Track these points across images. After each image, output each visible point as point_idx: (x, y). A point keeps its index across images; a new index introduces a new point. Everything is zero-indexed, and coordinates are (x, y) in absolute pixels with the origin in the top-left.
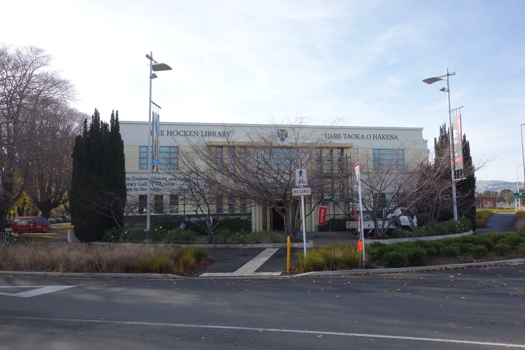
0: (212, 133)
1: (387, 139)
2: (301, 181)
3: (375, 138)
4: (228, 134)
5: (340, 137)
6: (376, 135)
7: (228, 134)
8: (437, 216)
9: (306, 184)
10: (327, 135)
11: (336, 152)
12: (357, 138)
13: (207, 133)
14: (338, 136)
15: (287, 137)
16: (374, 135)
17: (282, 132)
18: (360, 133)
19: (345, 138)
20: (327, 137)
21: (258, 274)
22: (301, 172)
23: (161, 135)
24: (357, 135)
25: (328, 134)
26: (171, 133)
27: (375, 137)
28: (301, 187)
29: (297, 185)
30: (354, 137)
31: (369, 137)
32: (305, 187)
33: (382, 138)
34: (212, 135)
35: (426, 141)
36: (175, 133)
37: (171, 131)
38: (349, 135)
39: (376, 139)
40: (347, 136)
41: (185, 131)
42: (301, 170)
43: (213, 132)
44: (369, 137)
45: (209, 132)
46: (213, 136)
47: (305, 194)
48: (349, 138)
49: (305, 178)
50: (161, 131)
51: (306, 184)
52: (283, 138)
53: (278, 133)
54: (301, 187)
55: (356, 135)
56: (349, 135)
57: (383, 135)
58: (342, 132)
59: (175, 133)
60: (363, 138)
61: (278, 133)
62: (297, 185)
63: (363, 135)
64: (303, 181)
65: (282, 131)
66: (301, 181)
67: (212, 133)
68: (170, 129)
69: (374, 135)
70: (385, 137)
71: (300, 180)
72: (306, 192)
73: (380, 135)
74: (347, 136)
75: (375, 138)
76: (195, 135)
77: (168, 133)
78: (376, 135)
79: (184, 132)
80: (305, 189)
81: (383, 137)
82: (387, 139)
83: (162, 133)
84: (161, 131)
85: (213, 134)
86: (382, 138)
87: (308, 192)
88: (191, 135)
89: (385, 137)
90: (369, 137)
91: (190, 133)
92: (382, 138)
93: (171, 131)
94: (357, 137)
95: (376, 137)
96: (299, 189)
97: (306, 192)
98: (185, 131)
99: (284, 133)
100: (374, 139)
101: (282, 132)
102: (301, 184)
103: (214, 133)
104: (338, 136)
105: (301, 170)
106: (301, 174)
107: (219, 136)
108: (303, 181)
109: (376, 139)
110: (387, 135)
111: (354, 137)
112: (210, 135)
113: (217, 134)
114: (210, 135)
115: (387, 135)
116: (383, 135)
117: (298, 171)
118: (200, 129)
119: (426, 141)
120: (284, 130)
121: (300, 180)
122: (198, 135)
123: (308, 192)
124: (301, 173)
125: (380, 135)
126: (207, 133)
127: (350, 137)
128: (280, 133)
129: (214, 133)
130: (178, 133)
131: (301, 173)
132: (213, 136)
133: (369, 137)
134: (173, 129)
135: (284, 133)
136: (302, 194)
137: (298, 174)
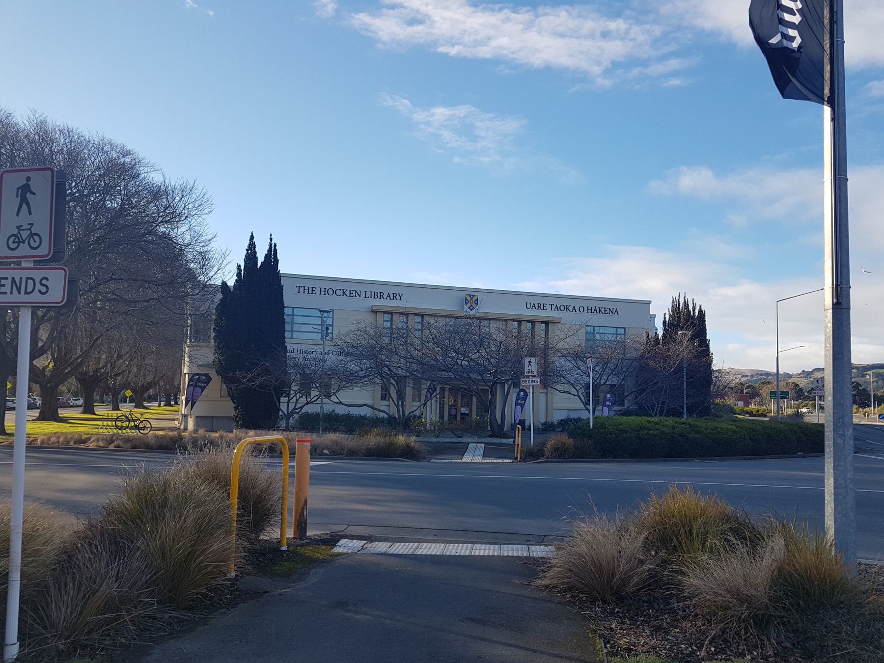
0: (379, 295)
1: (605, 313)
2: (530, 371)
3: (590, 311)
4: (400, 297)
5: (545, 308)
6: (591, 307)
7: (400, 297)
8: (655, 433)
9: (535, 374)
10: (528, 304)
11: (540, 328)
12: (567, 311)
13: (373, 293)
14: (542, 307)
15: (477, 304)
16: (588, 307)
17: (472, 298)
18: (571, 304)
19: (551, 310)
20: (528, 307)
21: (624, 419)
22: (530, 362)
23: (312, 293)
24: (567, 306)
25: (530, 303)
26: (325, 291)
27: (589, 310)
28: (24, 265)
29: (526, 374)
30: (562, 308)
31: (581, 309)
32: (533, 377)
33: (598, 312)
34: (379, 297)
35: (654, 316)
36: (331, 292)
37: (325, 289)
38: (557, 305)
39: (591, 312)
40: (554, 307)
41: (343, 290)
42: (28, 179)
43: (380, 293)
44: (581, 309)
45: (374, 292)
46: (380, 298)
47: (534, 384)
48: (556, 309)
49: (534, 367)
50: (312, 288)
51: (535, 374)
52: (471, 306)
53: (466, 299)
54: (19, 263)
55: (566, 307)
56: (557, 305)
57: (599, 308)
58: (548, 302)
59: (331, 292)
60: (574, 311)
61: (466, 299)
62: (526, 374)
63: (574, 307)
64: (32, 235)
65: (472, 297)
66: (530, 371)
67: (379, 295)
68: (324, 285)
69: (588, 307)
70: (603, 310)
71: (18, 227)
72: (13, 280)
73: (595, 308)
74: (554, 307)
75: (590, 311)
76: (357, 295)
77: (321, 291)
78: (591, 307)
79: (342, 291)
80: (534, 379)
81: (600, 310)
82: (605, 313)
83: (312, 290)
84: (312, 288)
85: (380, 296)
86: (598, 312)
87: (44, 289)
88: (351, 295)
89: (603, 310)
90: (581, 309)
91: (350, 293)
92: (598, 312)
93: (325, 289)
94: (567, 308)
95: (591, 310)
96: (528, 379)
97: (13, 280)
98: (343, 290)
99: (474, 299)
100: (588, 312)
101: (472, 298)
102: (530, 374)
103: (382, 294)
104: (542, 307)
105: (28, 179)
106: (24, 200)
107: (388, 298)
108: (32, 235)
109: (591, 312)
110: (605, 308)
111: (562, 308)
112: (376, 297)
113: (385, 296)
114: (376, 297)
115: (605, 308)
116: (599, 308)
117: (527, 360)
118: (362, 288)
119: (654, 316)
120: (474, 296)
121: (18, 227)
122: (360, 296)
123: (44, 289)
124: (29, 195)
125: (595, 308)
126: (373, 293)
127: (557, 308)
128: (469, 299)
129: (382, 294)
130: (334, 292)
131: (29, 195)
132: (380, 298)
133: (581, 309)
134: (328, 286)
135: (474, 299)
136: (530, 384)
137: (526, 364)
